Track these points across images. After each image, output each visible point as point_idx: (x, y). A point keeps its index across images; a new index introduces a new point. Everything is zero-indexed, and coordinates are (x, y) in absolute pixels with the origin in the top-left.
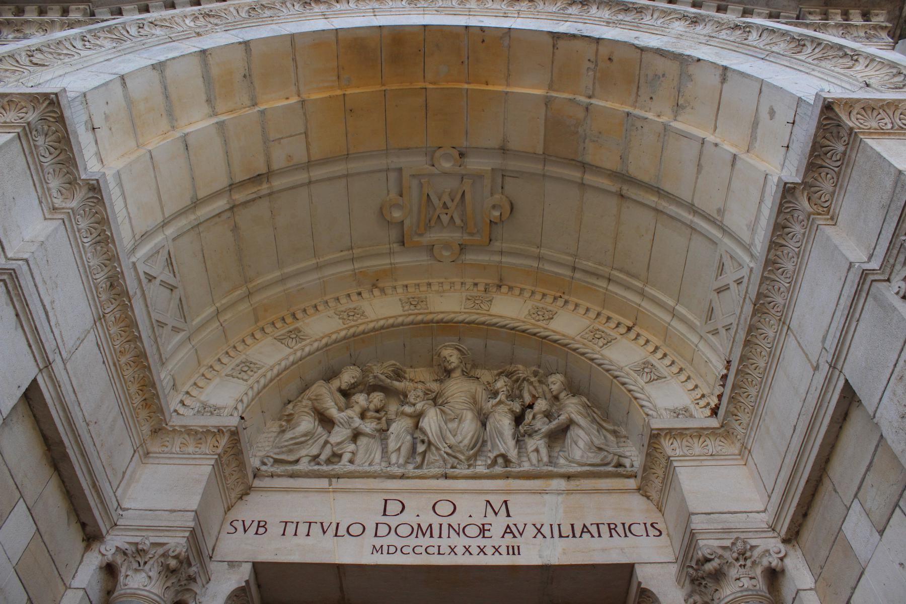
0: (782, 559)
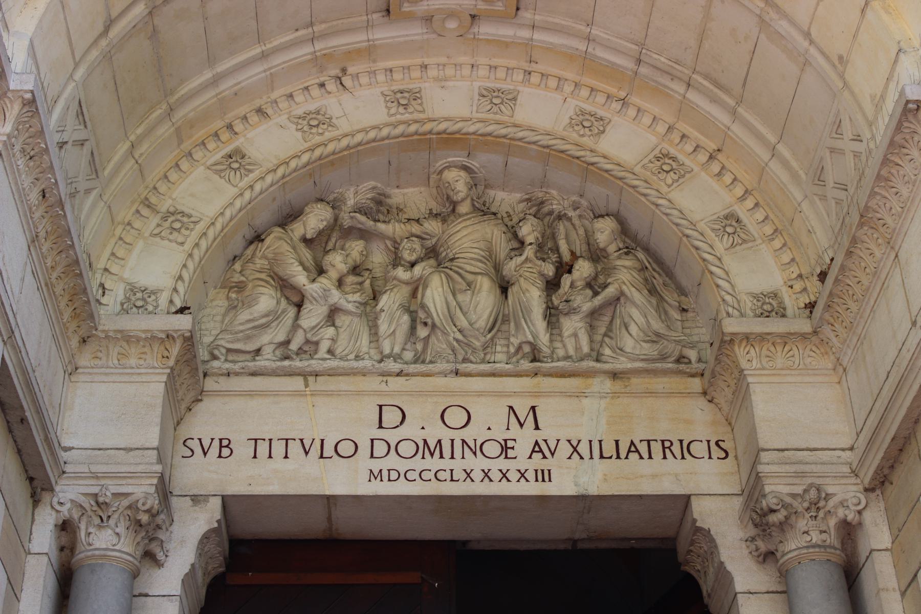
0: (860, 512)
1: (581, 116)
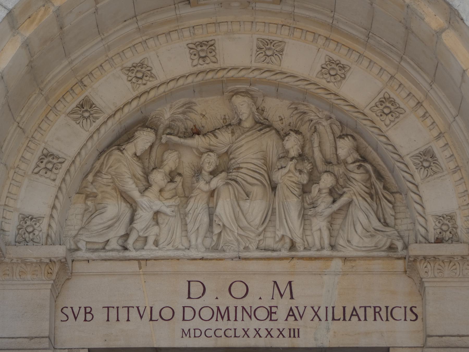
1: (329, 66)
